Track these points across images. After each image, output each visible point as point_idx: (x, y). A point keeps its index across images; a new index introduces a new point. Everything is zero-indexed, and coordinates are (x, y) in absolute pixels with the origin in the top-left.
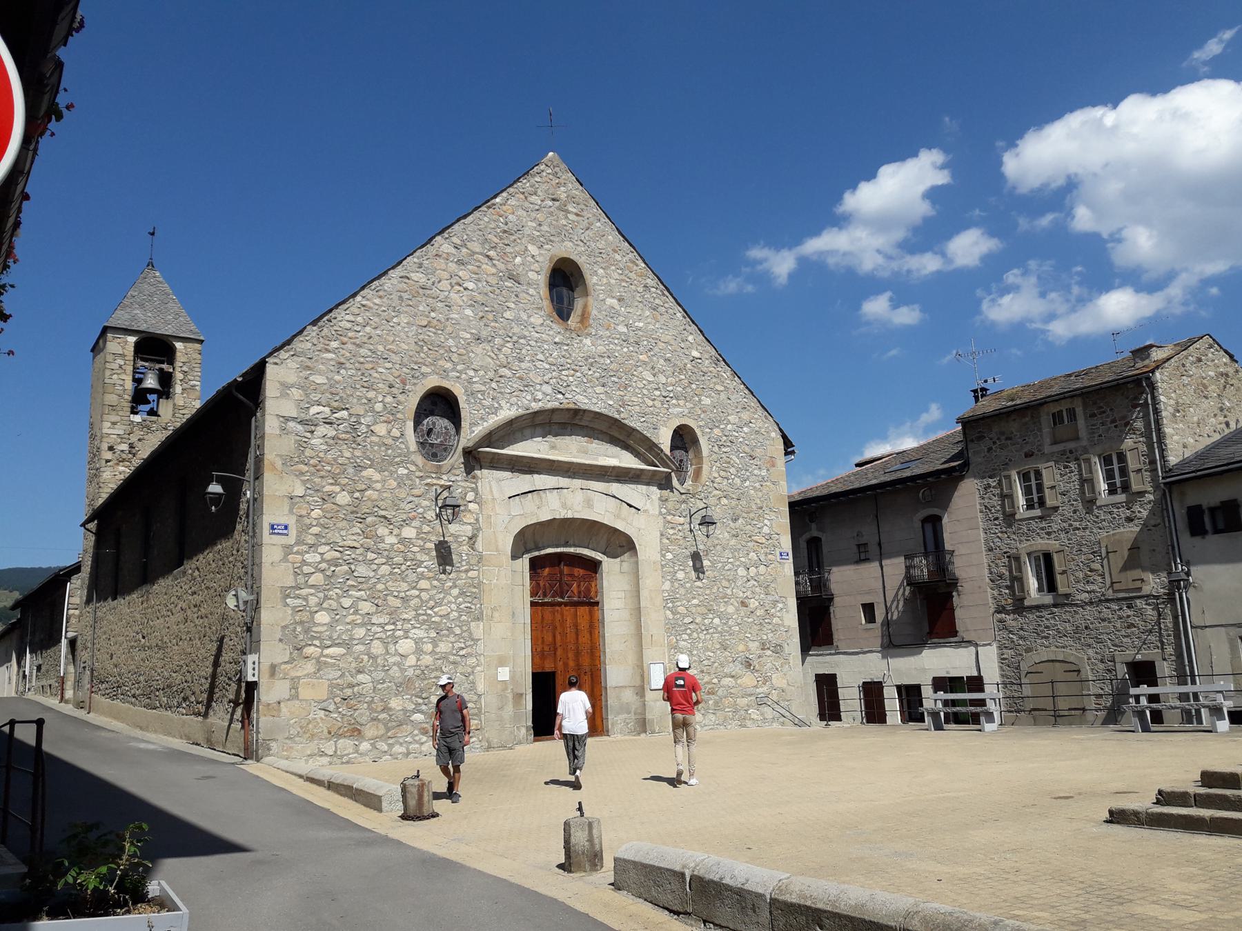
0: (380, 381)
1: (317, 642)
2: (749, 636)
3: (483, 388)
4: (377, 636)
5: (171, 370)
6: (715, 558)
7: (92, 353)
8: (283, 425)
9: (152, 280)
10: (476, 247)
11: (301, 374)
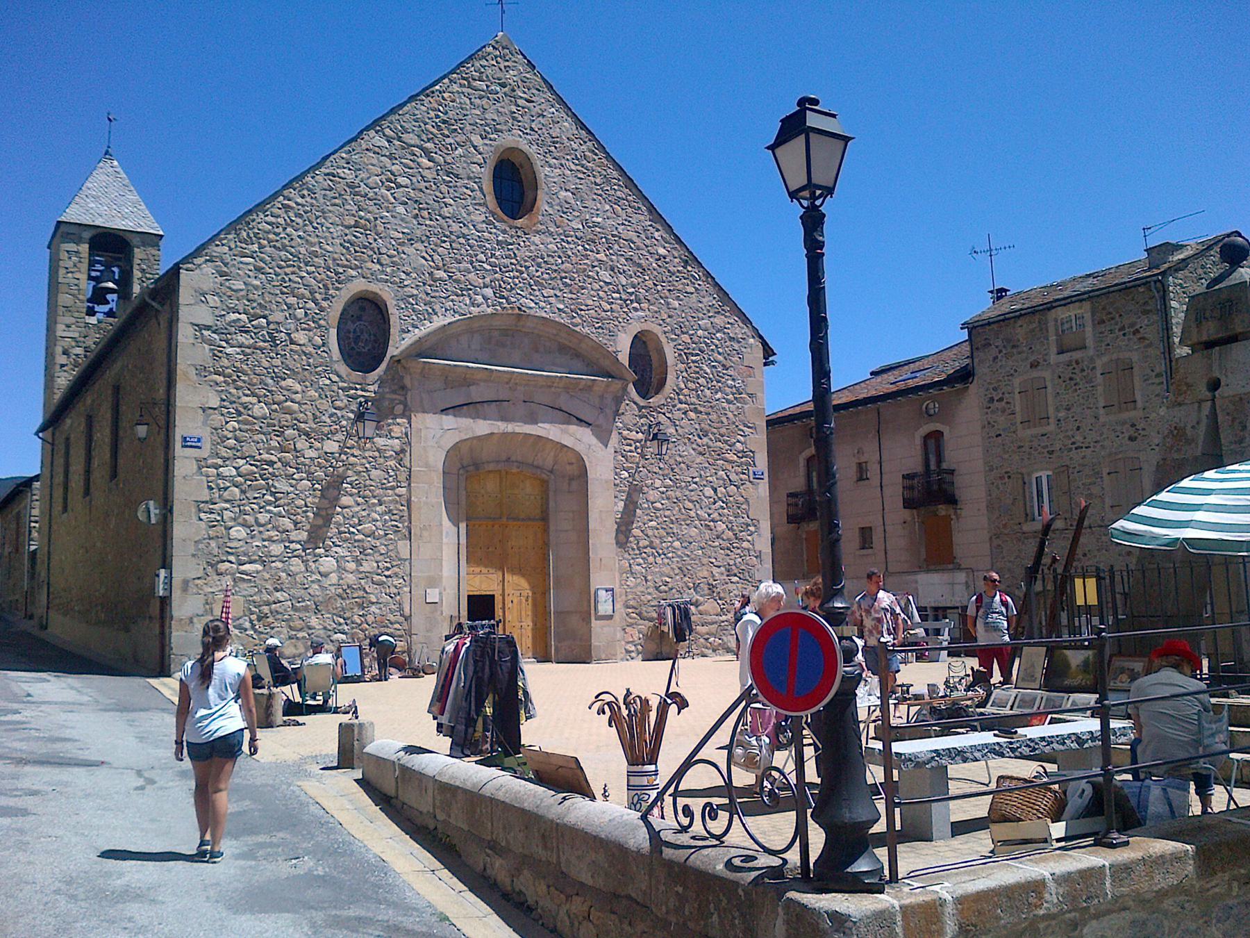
0: (301, 286)
1: (232, 558)
2: (714, 560)
3: (415, 292)
4: (295, 553)
6: (678, 477)
7: (49, 250)
10: (411, 138)
11: (216, 280)
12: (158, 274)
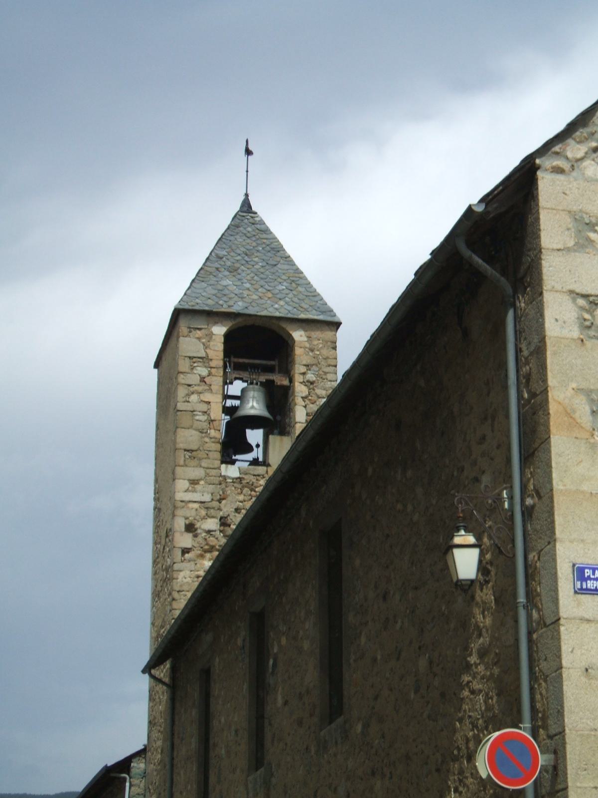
5: (286, 382)
7: (156, 370)
8: (587, 316)
9: (249, 229)
12: (261, 486)
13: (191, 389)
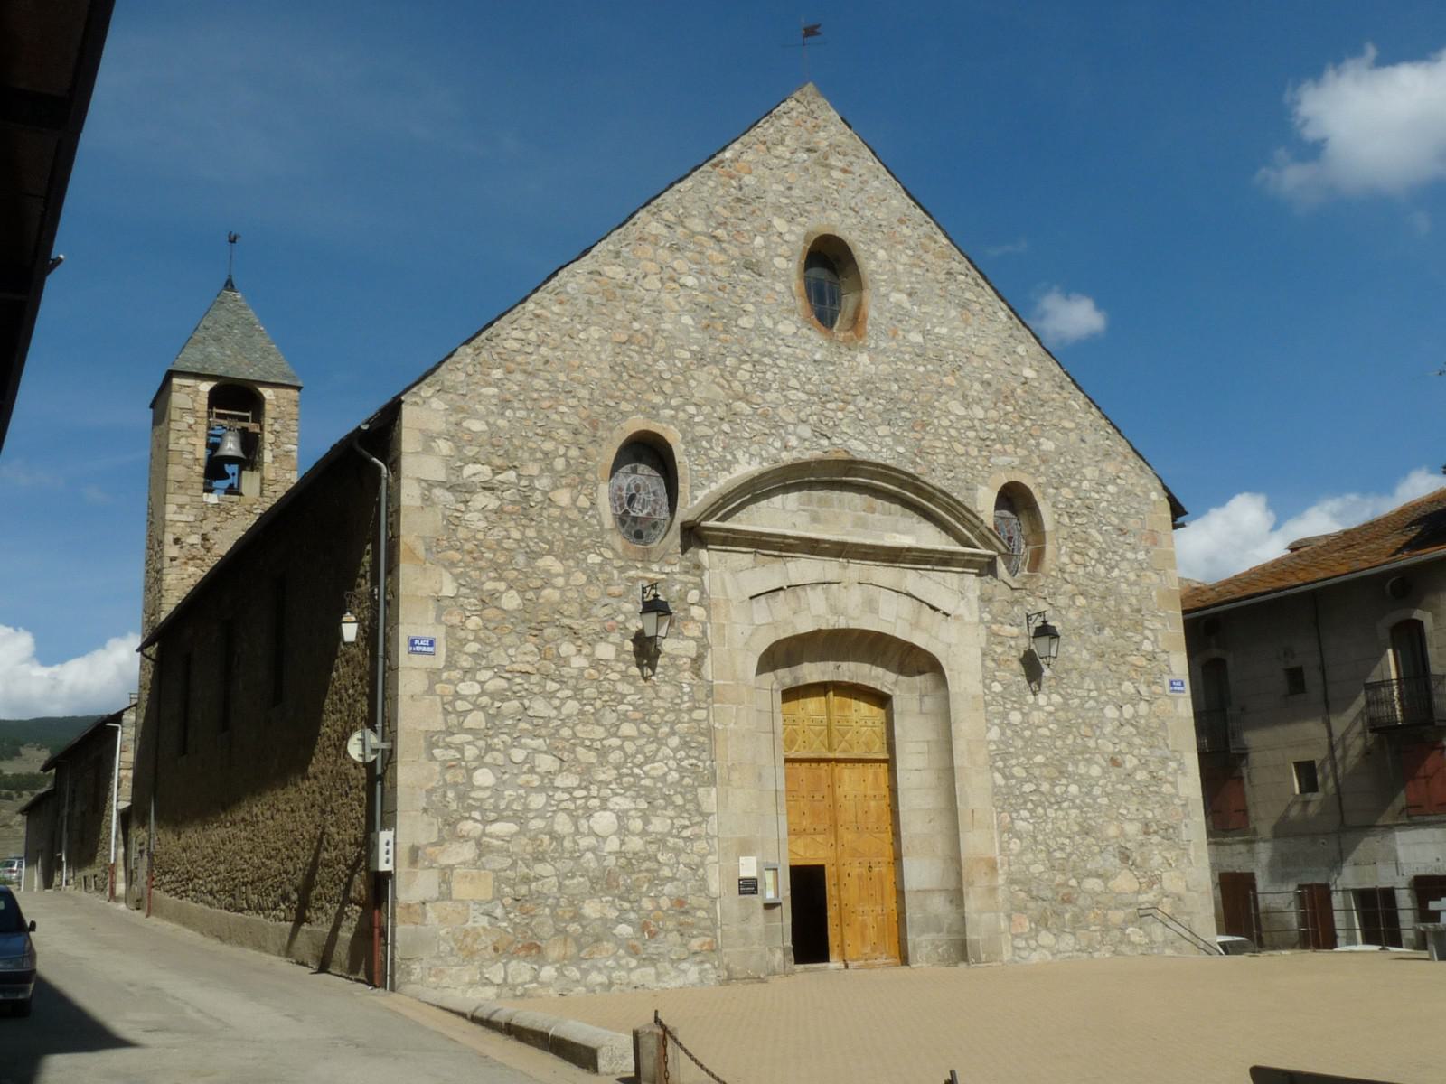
5: (258, 430)
13: (181, 433)
